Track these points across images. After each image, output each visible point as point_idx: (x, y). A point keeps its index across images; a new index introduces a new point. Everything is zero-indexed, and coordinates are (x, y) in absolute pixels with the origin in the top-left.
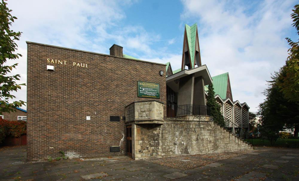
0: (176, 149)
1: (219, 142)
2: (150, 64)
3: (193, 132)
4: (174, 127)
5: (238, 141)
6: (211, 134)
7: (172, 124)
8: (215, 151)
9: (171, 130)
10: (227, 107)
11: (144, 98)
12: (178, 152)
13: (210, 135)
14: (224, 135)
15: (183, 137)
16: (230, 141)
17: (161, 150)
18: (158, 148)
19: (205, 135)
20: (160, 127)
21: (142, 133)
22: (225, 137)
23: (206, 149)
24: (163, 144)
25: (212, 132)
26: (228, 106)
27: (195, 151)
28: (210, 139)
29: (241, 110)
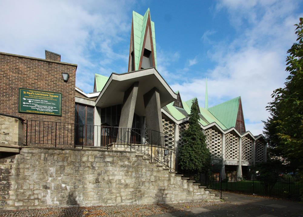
0: (49, 195)
1: (145, 186)
2: (45, 63)
3: (87, 169)
4: (46, 159)
5: (188, 185)
6: (128, 172)
7: (41, 153)
8: (136, 201)
9: (37, 163)
10: (231, 139)
11: (30, 115)
12: (53, 201)
13: (126, 175)
14: (158, 175)
15: (65, 177)
16: (170, 186)
17: (13, 197)
18: (8, 194)
19: (114, 175)
20: (14, 158)
22: (159, 179)
23: (116, 197)
24: (20, 186)
25: (131, 170)
26: (234, 138)
27: (91, 201)
28: (125, 181)
29: (255, 144)
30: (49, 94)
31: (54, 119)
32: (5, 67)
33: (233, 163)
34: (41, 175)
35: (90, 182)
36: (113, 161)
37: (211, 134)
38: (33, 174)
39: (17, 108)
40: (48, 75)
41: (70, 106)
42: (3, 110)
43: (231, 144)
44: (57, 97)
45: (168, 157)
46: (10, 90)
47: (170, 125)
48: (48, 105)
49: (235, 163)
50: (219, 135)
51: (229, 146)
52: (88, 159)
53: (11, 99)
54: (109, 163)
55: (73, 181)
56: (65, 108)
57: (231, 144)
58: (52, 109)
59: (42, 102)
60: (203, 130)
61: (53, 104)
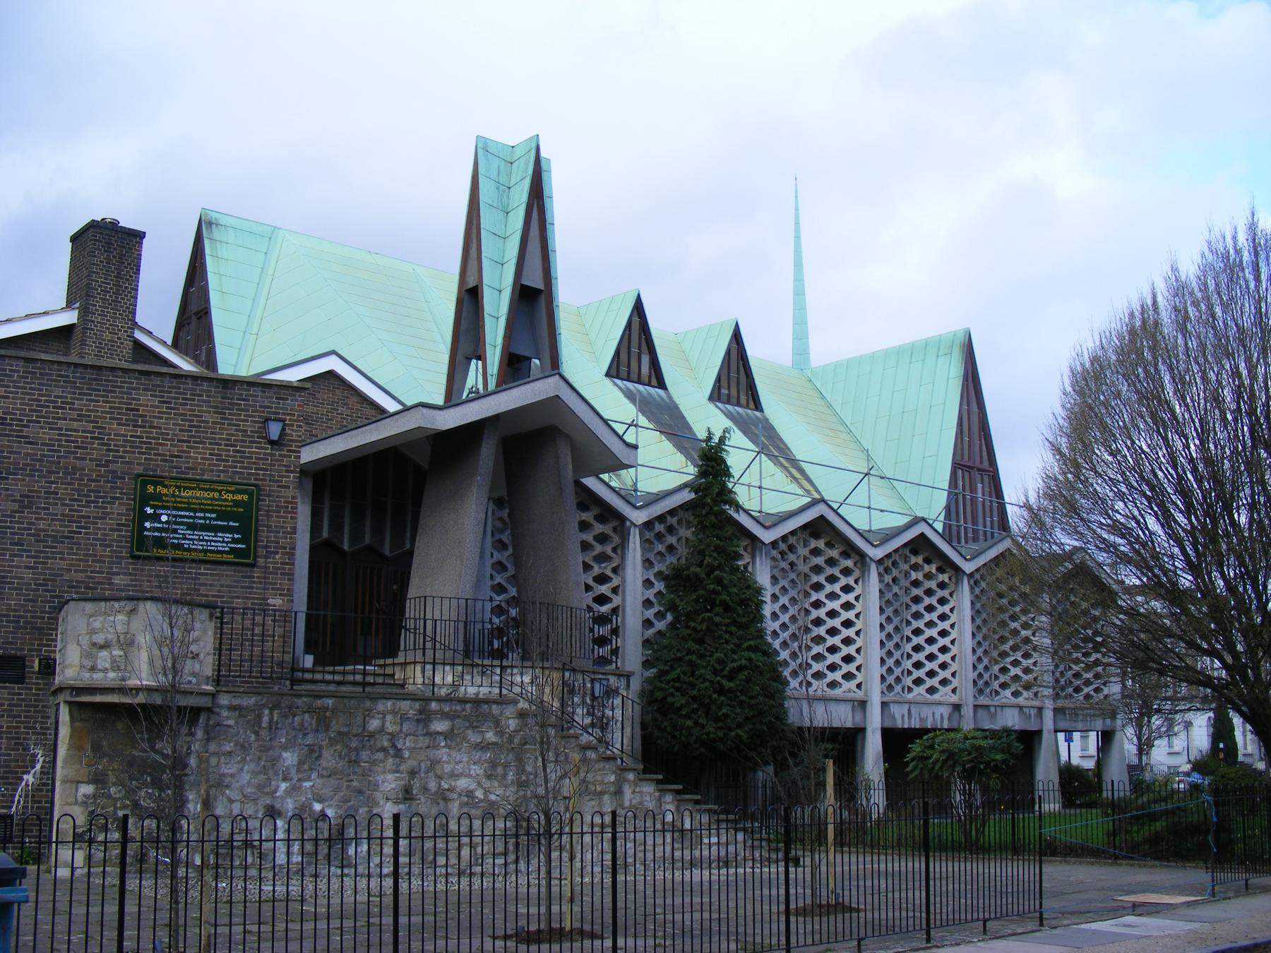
3: (380, 755)
9: (253, 737)
10: (916, 583)
13: (489, 777)
15: (319, 781)
19: (454, 776)
21: (96, 748)
30: (220, 492)
31: (231, 576)
32: (100, 406)
33: (930, 719)
34: (260, 772)
35: (387, 799)
36: (452, 730)
37: (805, 559)
38: (242, 769)
39: (126, 542)
40: (219, 423)
41: (283, 527)
42: (85, 550)
43: (914, 608)
44: (246, 497)
45: (603, 705)
46: (108, 482)
47: (599, 528)
48: (216, 529)
49: (938, 716)
50: (849, 563)
51: (908, 623)
52: (383, 726)
53: (109, 513)
54: (441, 738)
55: (342, 794)
56: (267, 537)
57: (914, 608)
58: (227, 543)
59: (201, 518)
60: (763, 543)
61: (231, 523)
